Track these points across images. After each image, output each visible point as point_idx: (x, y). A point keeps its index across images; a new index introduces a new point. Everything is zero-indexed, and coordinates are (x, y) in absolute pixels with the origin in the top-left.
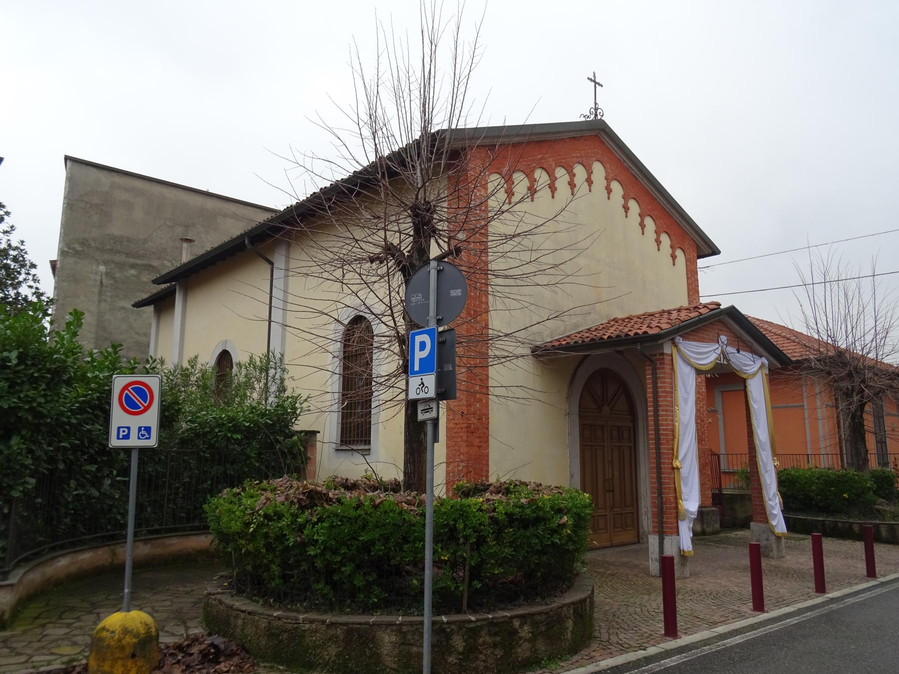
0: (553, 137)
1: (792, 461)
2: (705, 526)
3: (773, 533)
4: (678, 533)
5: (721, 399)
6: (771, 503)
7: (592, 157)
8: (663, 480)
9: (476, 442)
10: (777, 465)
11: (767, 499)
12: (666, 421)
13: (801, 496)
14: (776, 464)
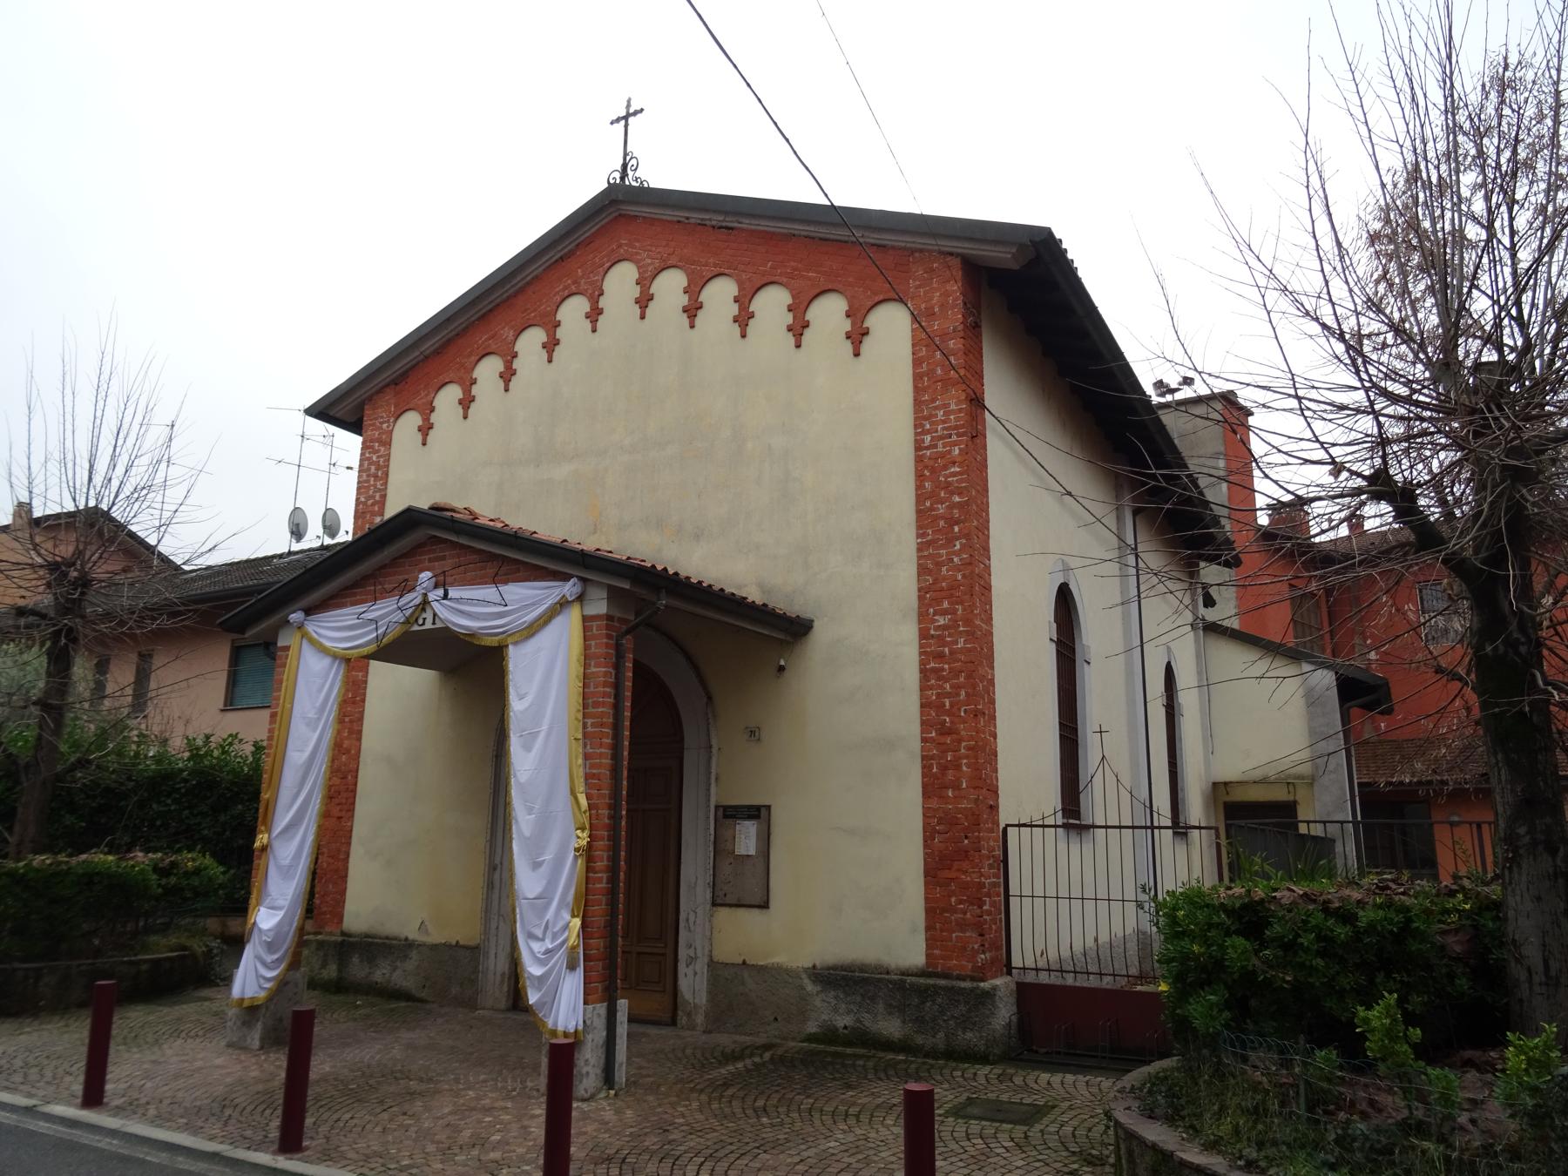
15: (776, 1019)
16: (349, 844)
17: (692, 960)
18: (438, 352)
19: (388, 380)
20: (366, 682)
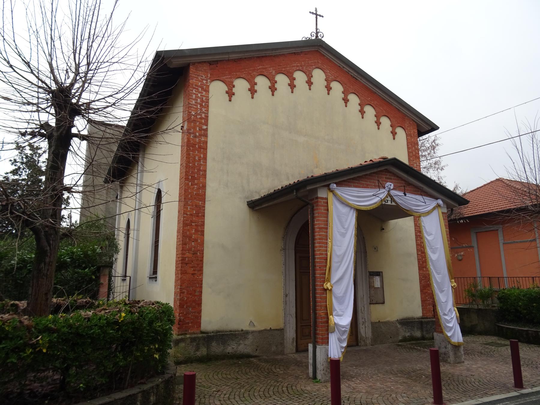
0: (274, 53)
1: (513, 283)
2: (425, 333)
3: (449, 342)
4: (327, 343)
5: (475, 239)
6: (446, 317)
7: (312, 66)
8: (317, 300)
9: (191, 271)
10: (454, 286)
11: (441, 314)
12: (319, 251)
13: (512, 310)
14: (453, 285)
15: (391, 337)
16: (201, 287)
17: (364, 323)
18: (235, 61)
19: (207, 60)
20: (204, 207)
